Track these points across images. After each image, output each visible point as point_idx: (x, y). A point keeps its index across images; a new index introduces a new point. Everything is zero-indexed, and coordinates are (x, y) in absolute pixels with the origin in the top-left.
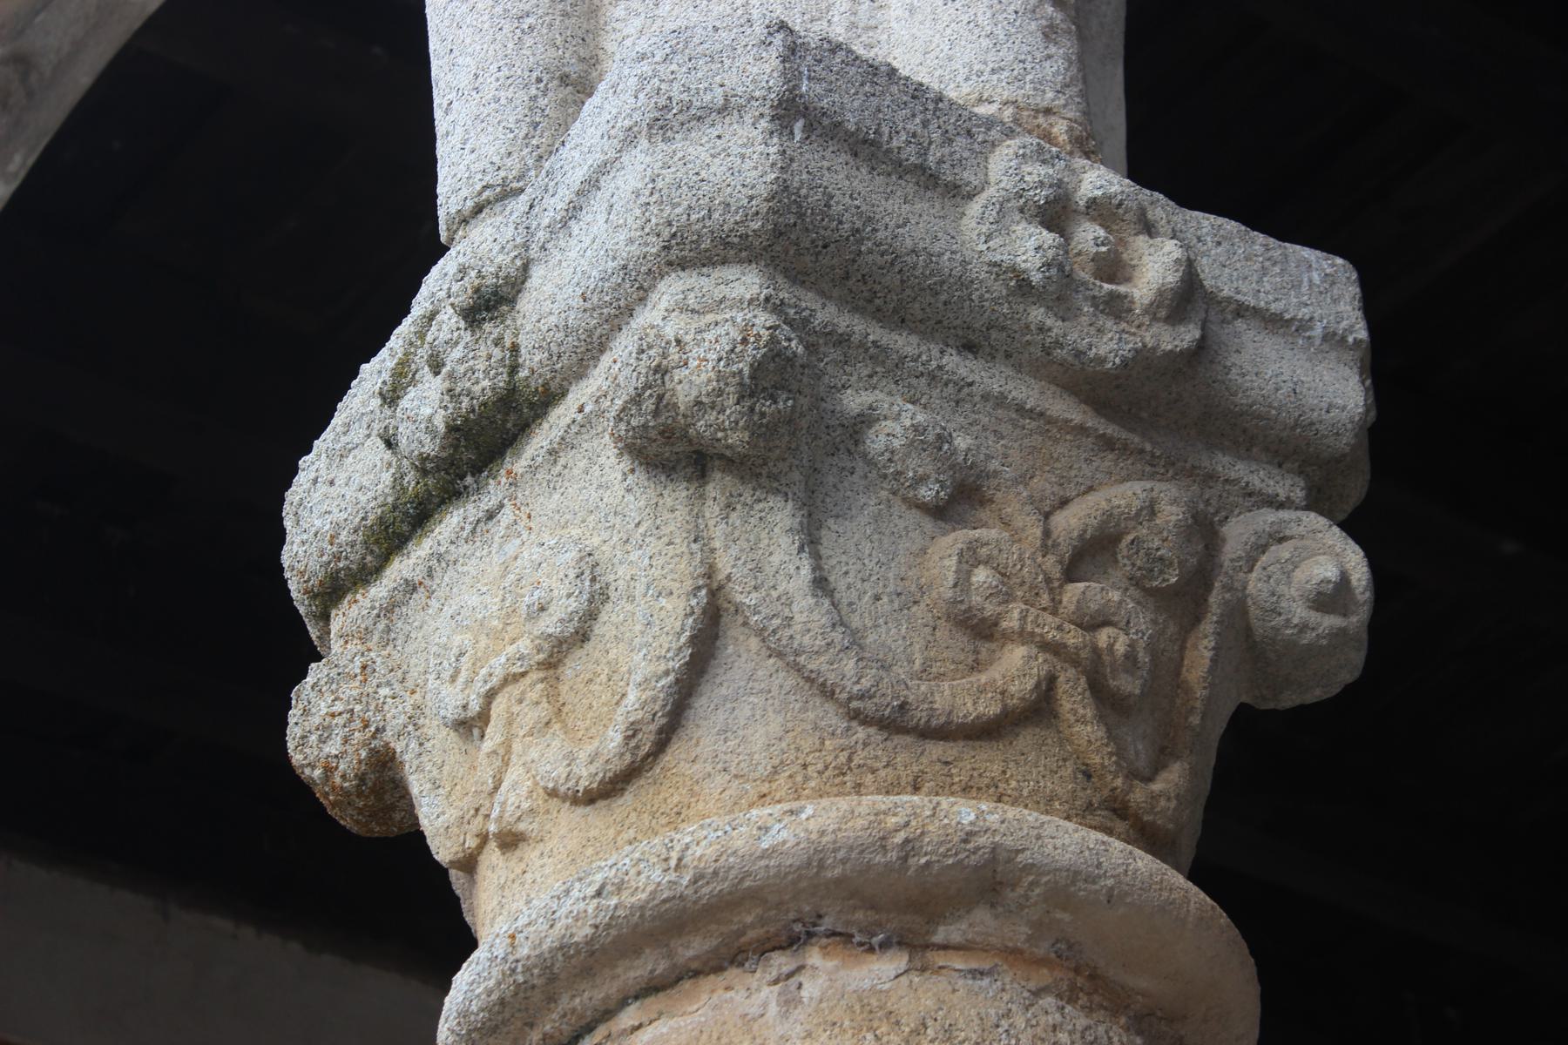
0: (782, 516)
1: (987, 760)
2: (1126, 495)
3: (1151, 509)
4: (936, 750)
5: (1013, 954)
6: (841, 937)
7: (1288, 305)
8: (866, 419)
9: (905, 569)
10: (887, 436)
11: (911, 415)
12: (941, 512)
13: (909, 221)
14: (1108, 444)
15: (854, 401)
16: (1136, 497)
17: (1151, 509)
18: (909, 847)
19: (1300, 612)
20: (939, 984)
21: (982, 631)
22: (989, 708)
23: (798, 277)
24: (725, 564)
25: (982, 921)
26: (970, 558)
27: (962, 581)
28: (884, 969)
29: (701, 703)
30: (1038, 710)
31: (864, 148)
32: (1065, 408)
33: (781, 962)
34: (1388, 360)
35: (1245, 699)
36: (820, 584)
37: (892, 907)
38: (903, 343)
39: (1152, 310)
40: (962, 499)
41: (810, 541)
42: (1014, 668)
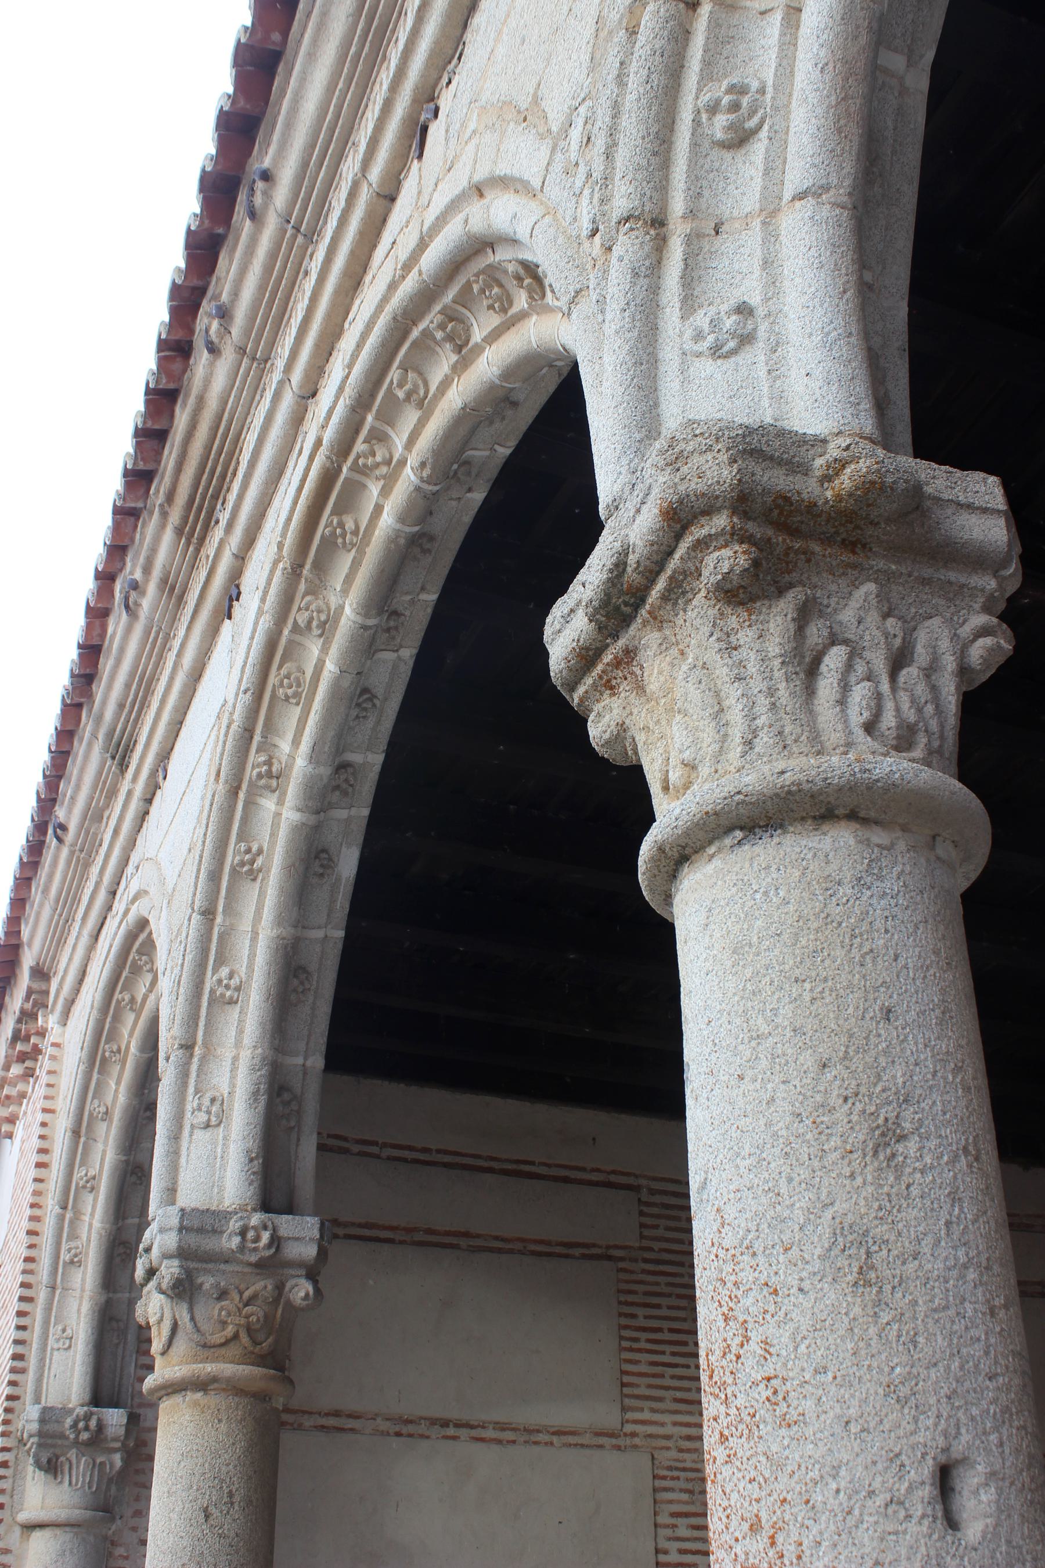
0: (185, 1306)
1: (222, 1351)
2: (262, 1283)
3: (266, 1287)
4: (212, 1350)
5: (224, 1390)
6: (192, 1390)
7: (302, 1234)
8: (201, 1285)
9: (209, 1311)
10: (207, 1286)
11: (212, 1280)
12: (219, 1299)
13: (209, 1244)
14: (258, 1274)
15: (199, 1280)
16: (262, 1286)
17: (266, 1287)
18: (198, 1377)
19: (299, 1301)
20: (209, 1397)
21: (224, 1323)
22: (223, 1340)
23: (186, 1259)
24: (177, 1317)
25: (216, 1385)
26: (221, 1309)
27: (220, 1314)
28: (199, 1395)
29: (174, 1341)
30: (236, 1336)
31: (200, 1230)
32: (247, 1270)
33: (183, 1393)
34: (1020, 510)
35: (964, 689)
36: (192, 1319)
37: (201, 1385)
38: (210, 1266)
39: (264, 1248)
40: (223, 1295)
41: (191, 1310)
42: (230, 1330)
